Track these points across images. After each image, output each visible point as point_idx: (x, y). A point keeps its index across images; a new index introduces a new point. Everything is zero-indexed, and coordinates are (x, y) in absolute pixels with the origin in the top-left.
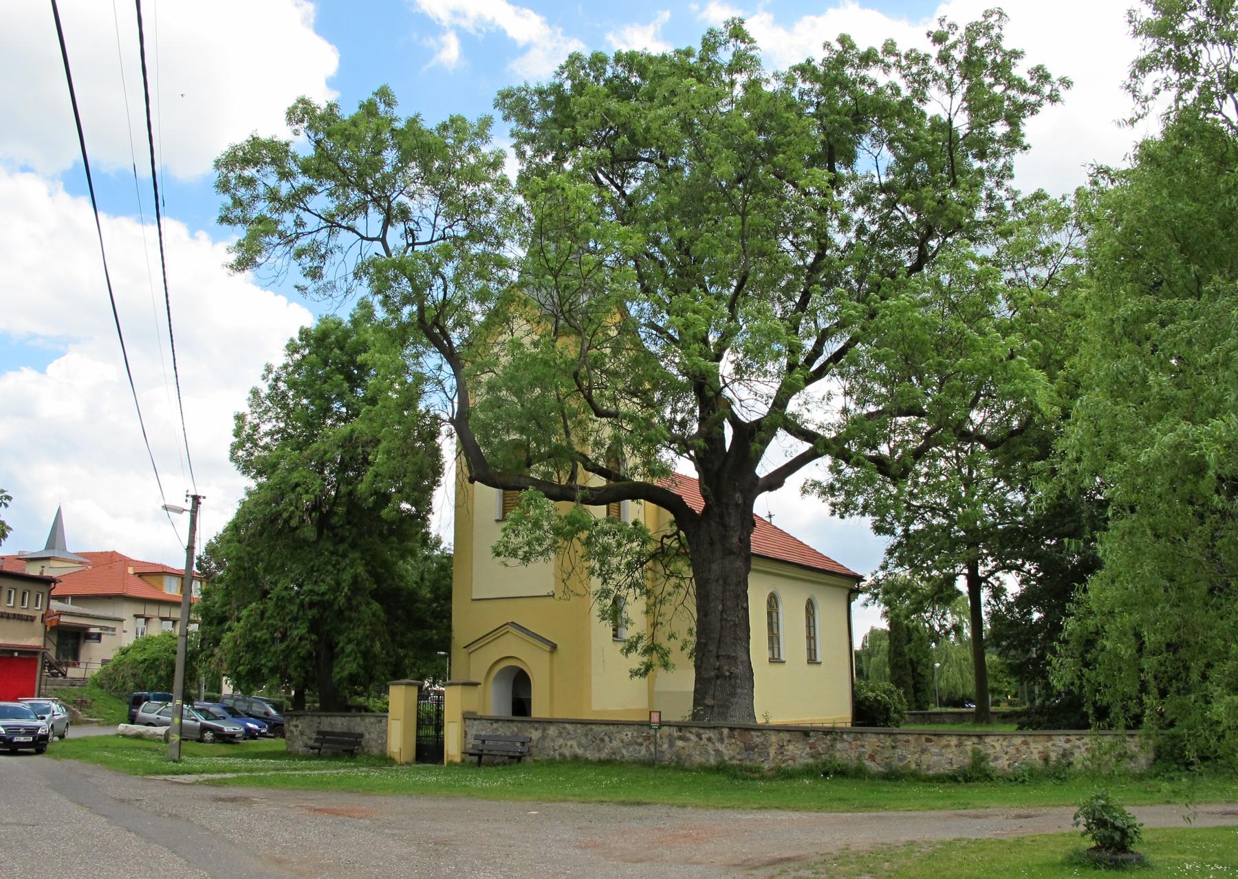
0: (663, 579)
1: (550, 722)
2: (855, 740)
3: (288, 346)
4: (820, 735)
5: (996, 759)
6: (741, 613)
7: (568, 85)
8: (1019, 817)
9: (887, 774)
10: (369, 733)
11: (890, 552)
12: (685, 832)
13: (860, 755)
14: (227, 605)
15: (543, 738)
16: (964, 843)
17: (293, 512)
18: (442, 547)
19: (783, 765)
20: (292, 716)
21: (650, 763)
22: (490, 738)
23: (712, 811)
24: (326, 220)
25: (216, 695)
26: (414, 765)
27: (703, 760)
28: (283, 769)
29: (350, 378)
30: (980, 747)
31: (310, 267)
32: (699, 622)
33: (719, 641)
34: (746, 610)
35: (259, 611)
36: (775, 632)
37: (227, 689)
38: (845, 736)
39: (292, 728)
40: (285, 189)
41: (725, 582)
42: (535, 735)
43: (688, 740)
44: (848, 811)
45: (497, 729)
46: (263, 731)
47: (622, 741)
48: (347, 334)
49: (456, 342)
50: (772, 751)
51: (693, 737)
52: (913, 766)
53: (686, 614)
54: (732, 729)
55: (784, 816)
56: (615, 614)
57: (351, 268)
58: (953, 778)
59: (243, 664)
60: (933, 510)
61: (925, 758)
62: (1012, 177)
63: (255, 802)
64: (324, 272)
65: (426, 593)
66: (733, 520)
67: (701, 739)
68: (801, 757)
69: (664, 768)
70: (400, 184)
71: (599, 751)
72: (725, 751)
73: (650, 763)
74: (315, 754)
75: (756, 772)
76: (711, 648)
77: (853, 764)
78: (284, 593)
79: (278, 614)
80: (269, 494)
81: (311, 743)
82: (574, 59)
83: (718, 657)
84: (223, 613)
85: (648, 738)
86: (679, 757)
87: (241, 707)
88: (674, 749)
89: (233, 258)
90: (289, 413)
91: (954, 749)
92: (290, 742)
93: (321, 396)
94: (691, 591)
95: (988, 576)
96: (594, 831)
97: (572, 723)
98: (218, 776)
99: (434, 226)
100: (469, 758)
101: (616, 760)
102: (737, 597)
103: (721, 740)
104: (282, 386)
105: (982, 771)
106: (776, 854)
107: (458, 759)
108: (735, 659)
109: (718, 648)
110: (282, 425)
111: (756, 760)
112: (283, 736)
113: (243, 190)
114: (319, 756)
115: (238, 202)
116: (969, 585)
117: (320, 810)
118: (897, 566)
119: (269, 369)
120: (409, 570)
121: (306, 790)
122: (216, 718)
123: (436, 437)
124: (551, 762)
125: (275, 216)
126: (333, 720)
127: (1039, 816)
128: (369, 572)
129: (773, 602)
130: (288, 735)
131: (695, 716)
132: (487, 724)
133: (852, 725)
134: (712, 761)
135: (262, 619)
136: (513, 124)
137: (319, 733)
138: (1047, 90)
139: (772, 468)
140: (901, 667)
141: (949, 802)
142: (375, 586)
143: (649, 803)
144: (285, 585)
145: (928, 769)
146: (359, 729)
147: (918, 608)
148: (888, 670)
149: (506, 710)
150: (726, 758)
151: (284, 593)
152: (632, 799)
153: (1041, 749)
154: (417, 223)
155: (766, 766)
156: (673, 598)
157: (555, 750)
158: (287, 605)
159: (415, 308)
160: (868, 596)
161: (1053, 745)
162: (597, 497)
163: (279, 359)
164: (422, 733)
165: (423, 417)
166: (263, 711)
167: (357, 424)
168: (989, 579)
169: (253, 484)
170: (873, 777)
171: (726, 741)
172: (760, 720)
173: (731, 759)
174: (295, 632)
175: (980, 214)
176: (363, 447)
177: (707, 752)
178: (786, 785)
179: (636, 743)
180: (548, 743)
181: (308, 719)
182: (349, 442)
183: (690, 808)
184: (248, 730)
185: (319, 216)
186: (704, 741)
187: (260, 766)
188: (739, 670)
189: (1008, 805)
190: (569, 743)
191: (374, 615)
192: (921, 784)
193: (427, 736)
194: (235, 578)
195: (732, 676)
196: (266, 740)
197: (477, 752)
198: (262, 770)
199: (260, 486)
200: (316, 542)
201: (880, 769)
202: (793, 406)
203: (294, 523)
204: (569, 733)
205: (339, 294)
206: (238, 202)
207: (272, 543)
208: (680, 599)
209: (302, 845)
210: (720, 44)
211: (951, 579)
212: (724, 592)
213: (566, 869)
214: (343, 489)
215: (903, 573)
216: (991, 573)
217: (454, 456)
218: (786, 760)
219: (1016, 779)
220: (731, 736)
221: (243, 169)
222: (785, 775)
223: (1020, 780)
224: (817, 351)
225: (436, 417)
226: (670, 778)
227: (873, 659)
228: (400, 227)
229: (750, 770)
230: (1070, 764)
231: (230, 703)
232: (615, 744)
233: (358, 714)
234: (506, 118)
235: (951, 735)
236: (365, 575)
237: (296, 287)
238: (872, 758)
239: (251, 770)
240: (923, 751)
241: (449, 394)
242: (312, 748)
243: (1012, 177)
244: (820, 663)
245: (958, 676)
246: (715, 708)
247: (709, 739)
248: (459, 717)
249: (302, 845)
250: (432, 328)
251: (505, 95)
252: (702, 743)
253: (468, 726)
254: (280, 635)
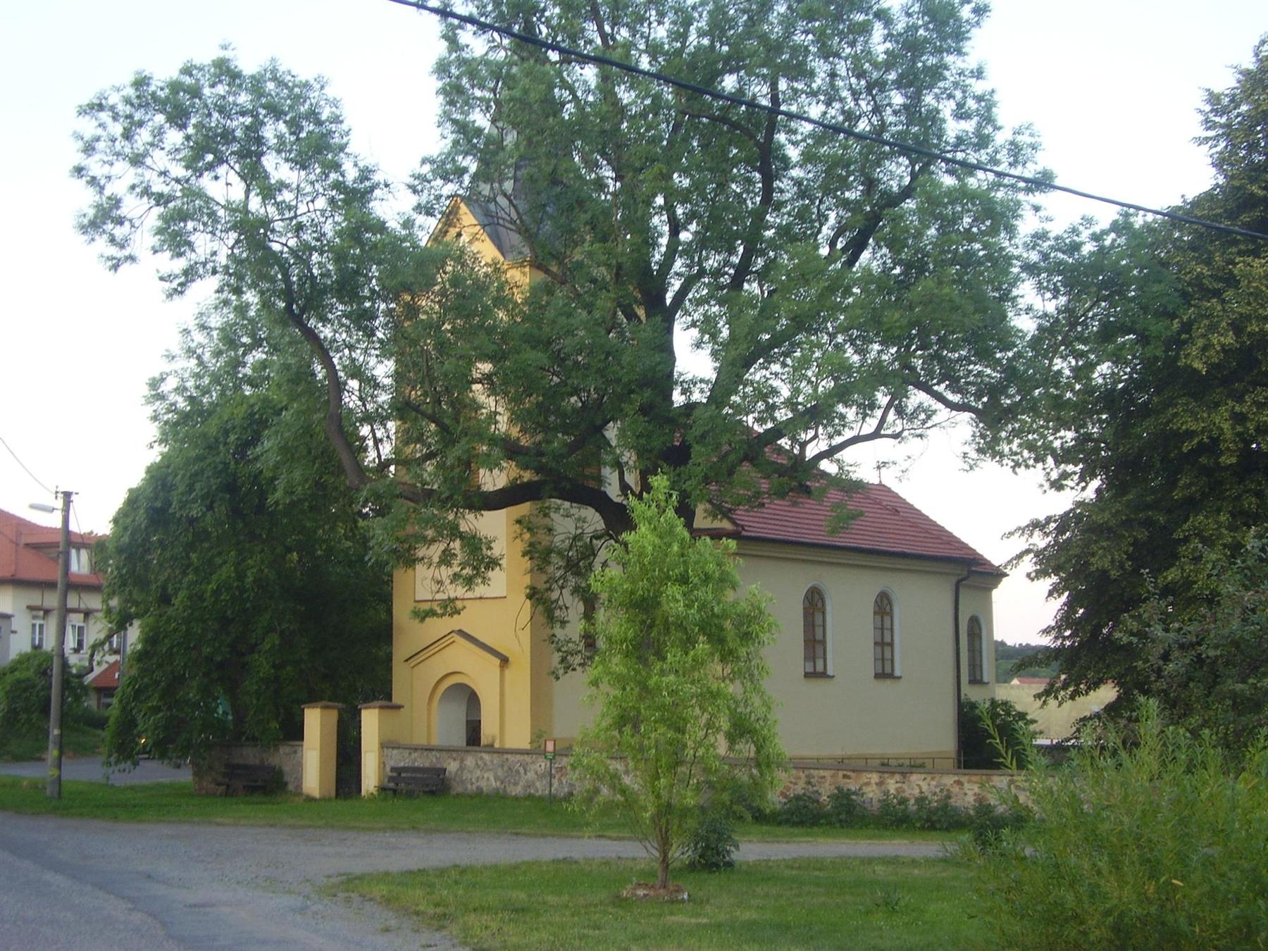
15: (462, 768)
91: (874, 787)
157: (472, 784)
204: (485, 764)
244: (899, 678)
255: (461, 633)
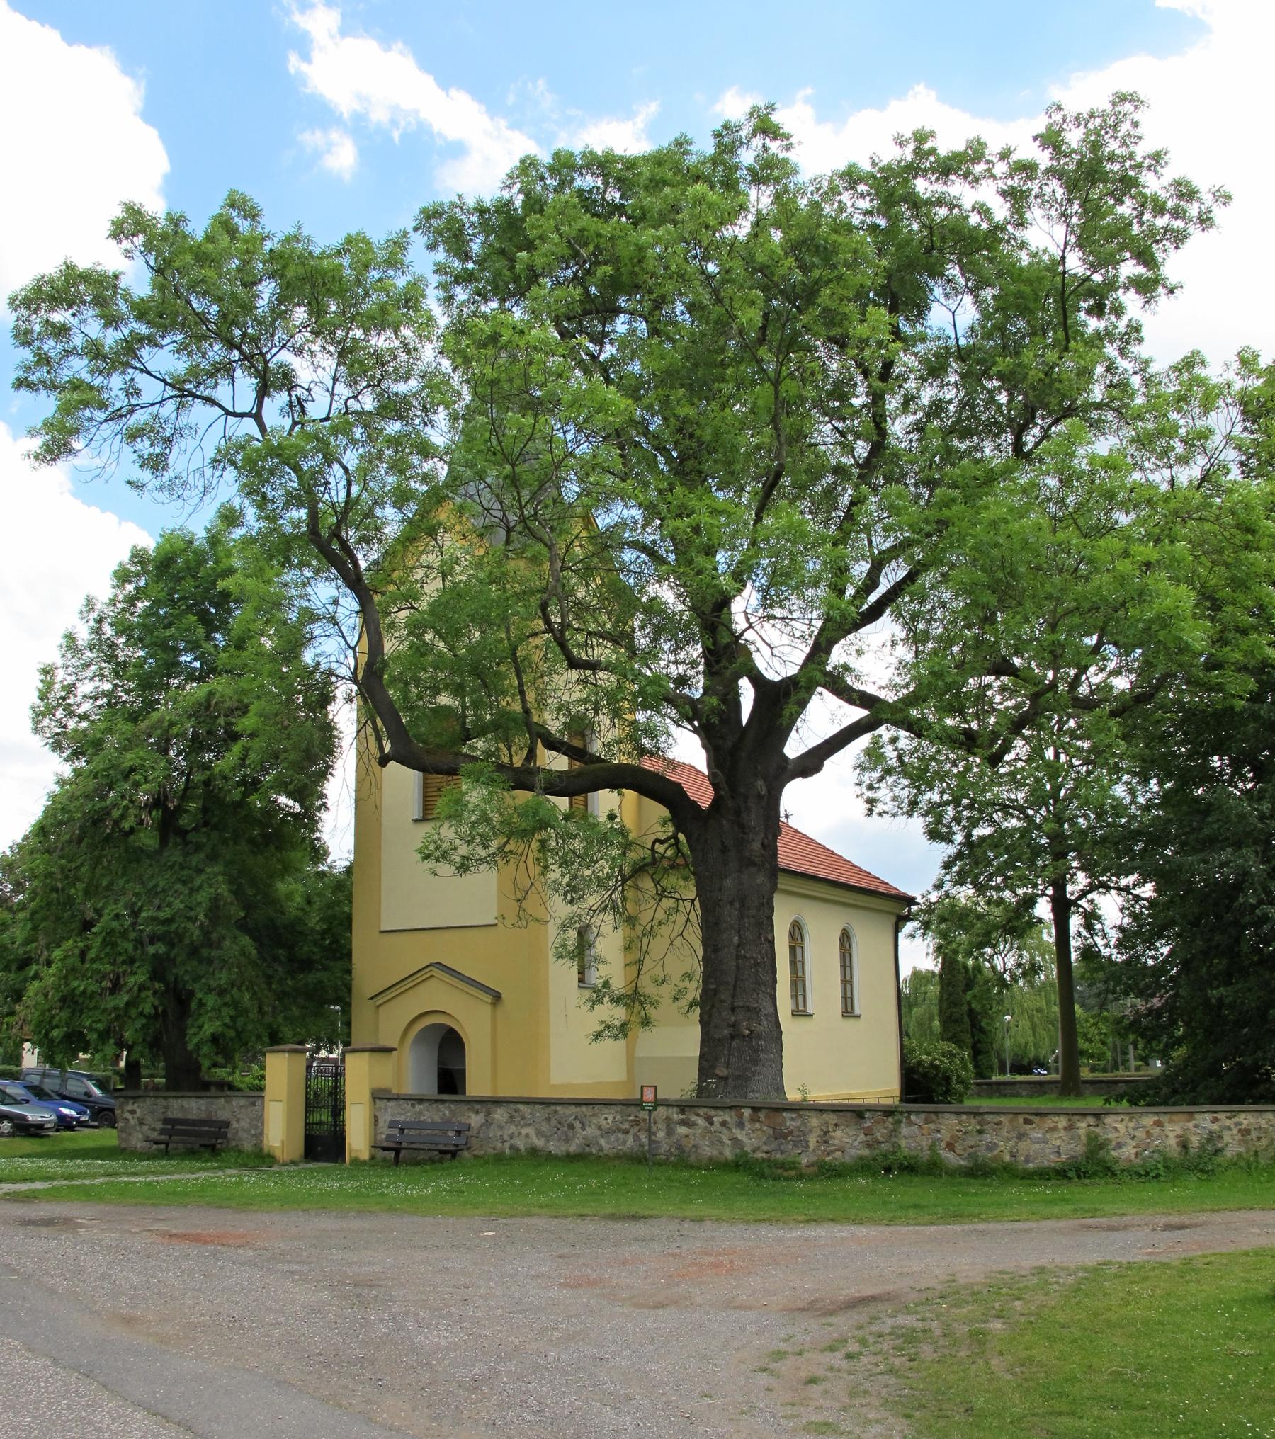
0: (653, 902)
1: (497, 1102)
2: (927, 1121)
3: (115, 574)
4: (880, 1116)
5: (1119, 1146)
6: (766, 946)
7: (519, 201)
8: (1169, 1227)
9: (972, 1169)
10: (238, 1121)
11: (947, 866)
12: (712, 1259)
13: (934, 1144)
14: (32, 942)
15: (487, 1124)
16: (1114, 1270)
17: (127, 808)
18: (329, 861)
19: (827, 1159)
20: (126, 1098)
21: (639, 1159)
22: (411, 1125)
23: (743, 1227)
24: (173, 386)
25: (14, 1068)
26: (302, 1166)
27: (715, 1152)
28: (117, 1174)
29: (205, 618)
30: (1097, 1130)
31: (150, 455)
32: (706, 959)
33: (735, 987)
34: (772, 943)
35: (77, 951)
36: (800, 974)
37: (30, 1058)
38: (913, 1117)
39: (127, 1115)
40: (111, 338)
41: (743, 905)
42: (475, 1120)
43: (694, 1124)
44: (932, 1224)
45: (421, 1113)
46: (83, 1118)
47: (600, 1128)
48: (201, 558)
49: (363, 565)
50: (812, 1141)
51: (701, 1121)
52: (1007, 1158)
53: (687, 951)
54: (755, 1109)
55: (843, 1232)
56: (581, 951)
57: (211, 453)
58: (1061, 1174)
59: (57, 1026)
60: (1005, 808)
61: (1023, 1146)
62: (1140, 340)
63: (82, 1226)
64: (171, 461)
65: (314, 922)
66: (754, 819)
67: (712, 1124)
68: (853, 1147)
69: (660, 1164)
70: (280, 335)
71: (567, 1141)
72: (745, 1139)
73: (639, 1159)
74: (160, 1151)
75: (791, 1169)
76: (723, 997)
77: (925, 1156)
78: (115, 924)
79: (107, 954)
80: (92, 784)
81: (155, 1135)
82: (528, 165)
83: (733, 1009)
84: (25, 953)
85: (636, 1123)
86: (680, 1148)
87: (50, 1085)
88: (675, 1138)
89: (36, 444)
90: (120, 670)
91: (1062, 1133)
92: (124, 1135)
93: (163, 646)
94: (693, 917)
95: (1080, 898)
96: (581, 1260)
97: (528, 1103)
98: (23, 1187)
99: (332, 395)
100: (381, 1154)
101: (591, 1154)
102: (759, 925)
103: (741, 1125)
104: (108, 631)
105: (1101, 1162)
106: (853, 1292)
107: (365, 1156)
108: (757, 1011)
109: (733, 996)
110: (108, 686)
111: (790, 1152)
112: (112, 1125)
113: (51, 343)
114: (166, 1154)
115: (43, 359)
116: (1054, 910)
117: (177, 1236)
118: (956, 884)
119: (90, 605)
120: (291, 891)
121: (154, 1205)
122: (16, 1102)
123: (329, 704)
124: (499, 1158)
125: (98, 381)
126: (185, 1103)
127: (1196, 1225)
128: (235, 893)
129: (797, 931)
130: (121, 1124)
131: (700, 1091)
132: (406, 1106)
133: (901, 1100)
134: (728, 1154)
135: (83, 962)
136: (440, 255)
137: (166, 1121)
138: (1193, 210)
139: (814, 741)
140: (956, 1021)
141: (1068, 1208)
142: (242, 914)
143: (651, 1217)
144: (112, 912)
145: (1027, 1161)
146: (223, 1115)
147: (986, 940)
148: (936, 1023)
149: (429, 1086)
150: (748, 1149)
151: (115, 924)
152: (624, 1210)
153: (1179, 1131)
154: (309, 390)
155: (804, 1160)
156: (665, 930)
157: (503, 1142)
158: (119, 941)
159: (303, 513)
160: (915, 924)
161: (1196, 1126)
162: (558, 785)
163: (104, 590)
164: (315, 1118)
165: (313, 672)
166: (83, 1090)
167: (219, 684)
168: (1080, 902)
169: (66, 770)
170: (953, 1173)
171: (748, 1126)
172: (792, 1095)
173: (754, 1151)
174: (132, 979)
175: (1098, 393)
176: (226, 716)
177: (721, 1142)
178: (834, 1186)
179: (620, 1130)
180: (493, 1132)
181: (149, 1101)
182: (205, 710)
183: (709, 1223)
184: (62, 1118)
185: (164, 381)
186: (717, 1126)
187: (84, 1170)
188: (763, 1027)
189: (1150, 1211)
190: (524, 1131)
191: (243, 953)
192: (1019, 1181)
193: (320, 1123)
194: (43, 904)
195: (753, 1035)
196: (87, 1131)
197: (392, 1145)
198: (85, 1176)
199: (78, 773)
200: (159, 852)
201: (962, 1162)
202: (838, 655)
203: (126, 825)
204: (523, 1118)
205: (193, 496)
206: (43, 359)
207: (96, 853)
208: (678, 929)
209: (159, 1293)
210: (742, 143)
211: (1030, 902)
212: (741, 917)
213: (556, 1322)
214: (198, 777)
215: (965, 894)
216: (1084, 894)
217: (354, 728)
218: (833, 1152)
219: (1147, 1174)
220: (754, 1120)
221: (52, 310)
222: (830, 1172)
223: (1152, 1174)
224: (871, 582)
225: (330, 673)
226: (669, 1179)
227: (914, 1011)
228: (281, 398)
229: (782, 1166)
230: (1218, 1152)
231: (35, 1080)
232: (591, 1131)
233: (220, 1094)
234: (431, 247)
235: (1058, 1114)
236: (230, 898)
237: (129, 482)
238: (950, 1147)
239: (71, 1177)
240: (1021, 1137)
241: (349, 639)
242: (157, 1143)
243: (1140, 340)
244: (858, 1016)
245: (1030, 1032)
246: (730, 1080)
247: (724, 1124)
248: (367, 1096)
249: (159, 1293)
250: (329, 542)
251: (430, 214)
252: (713, 1129)
253: (380, 1109)
254: (109, 985)
255: (439, 965)
